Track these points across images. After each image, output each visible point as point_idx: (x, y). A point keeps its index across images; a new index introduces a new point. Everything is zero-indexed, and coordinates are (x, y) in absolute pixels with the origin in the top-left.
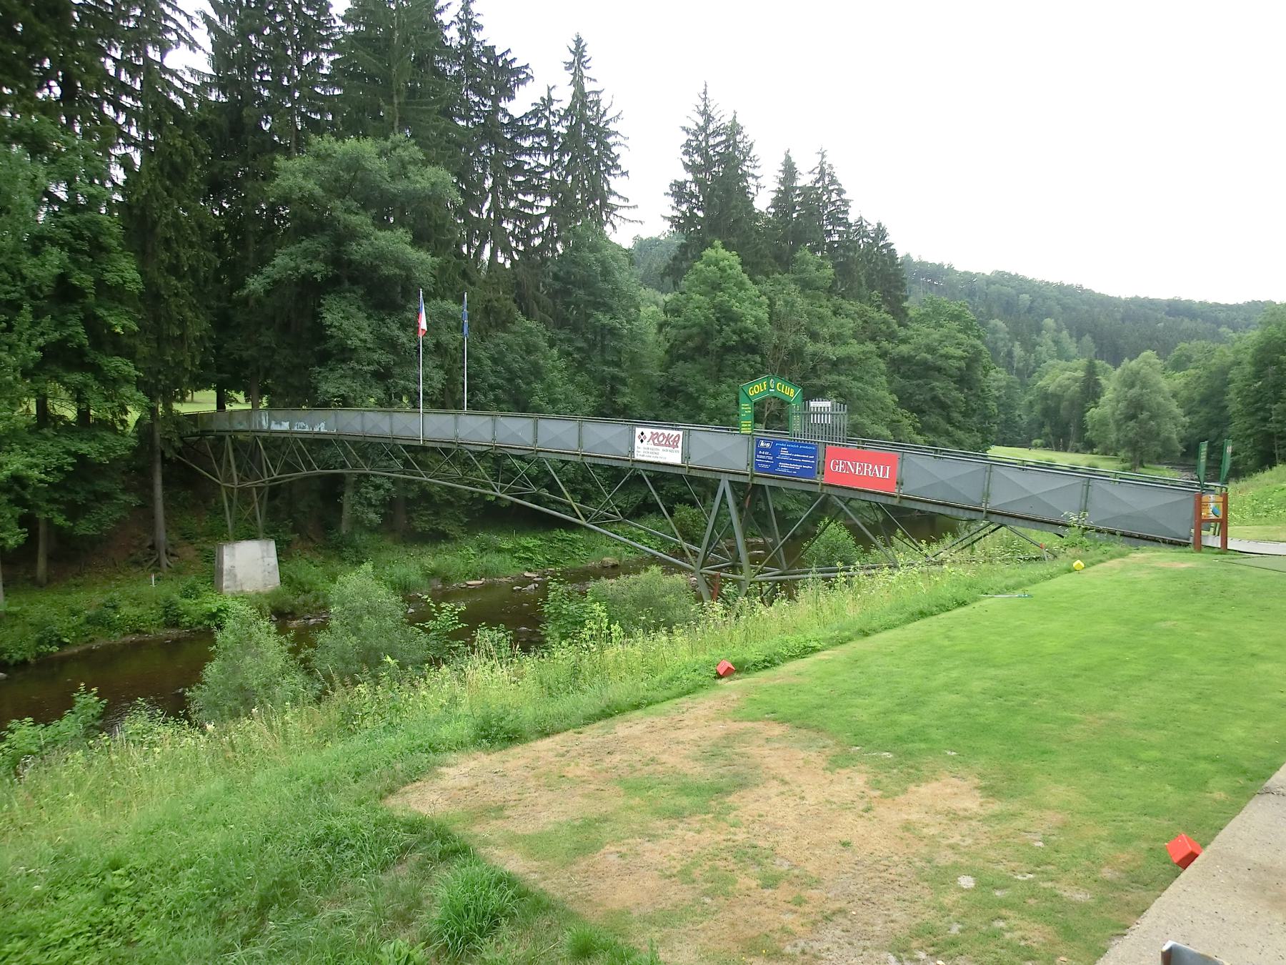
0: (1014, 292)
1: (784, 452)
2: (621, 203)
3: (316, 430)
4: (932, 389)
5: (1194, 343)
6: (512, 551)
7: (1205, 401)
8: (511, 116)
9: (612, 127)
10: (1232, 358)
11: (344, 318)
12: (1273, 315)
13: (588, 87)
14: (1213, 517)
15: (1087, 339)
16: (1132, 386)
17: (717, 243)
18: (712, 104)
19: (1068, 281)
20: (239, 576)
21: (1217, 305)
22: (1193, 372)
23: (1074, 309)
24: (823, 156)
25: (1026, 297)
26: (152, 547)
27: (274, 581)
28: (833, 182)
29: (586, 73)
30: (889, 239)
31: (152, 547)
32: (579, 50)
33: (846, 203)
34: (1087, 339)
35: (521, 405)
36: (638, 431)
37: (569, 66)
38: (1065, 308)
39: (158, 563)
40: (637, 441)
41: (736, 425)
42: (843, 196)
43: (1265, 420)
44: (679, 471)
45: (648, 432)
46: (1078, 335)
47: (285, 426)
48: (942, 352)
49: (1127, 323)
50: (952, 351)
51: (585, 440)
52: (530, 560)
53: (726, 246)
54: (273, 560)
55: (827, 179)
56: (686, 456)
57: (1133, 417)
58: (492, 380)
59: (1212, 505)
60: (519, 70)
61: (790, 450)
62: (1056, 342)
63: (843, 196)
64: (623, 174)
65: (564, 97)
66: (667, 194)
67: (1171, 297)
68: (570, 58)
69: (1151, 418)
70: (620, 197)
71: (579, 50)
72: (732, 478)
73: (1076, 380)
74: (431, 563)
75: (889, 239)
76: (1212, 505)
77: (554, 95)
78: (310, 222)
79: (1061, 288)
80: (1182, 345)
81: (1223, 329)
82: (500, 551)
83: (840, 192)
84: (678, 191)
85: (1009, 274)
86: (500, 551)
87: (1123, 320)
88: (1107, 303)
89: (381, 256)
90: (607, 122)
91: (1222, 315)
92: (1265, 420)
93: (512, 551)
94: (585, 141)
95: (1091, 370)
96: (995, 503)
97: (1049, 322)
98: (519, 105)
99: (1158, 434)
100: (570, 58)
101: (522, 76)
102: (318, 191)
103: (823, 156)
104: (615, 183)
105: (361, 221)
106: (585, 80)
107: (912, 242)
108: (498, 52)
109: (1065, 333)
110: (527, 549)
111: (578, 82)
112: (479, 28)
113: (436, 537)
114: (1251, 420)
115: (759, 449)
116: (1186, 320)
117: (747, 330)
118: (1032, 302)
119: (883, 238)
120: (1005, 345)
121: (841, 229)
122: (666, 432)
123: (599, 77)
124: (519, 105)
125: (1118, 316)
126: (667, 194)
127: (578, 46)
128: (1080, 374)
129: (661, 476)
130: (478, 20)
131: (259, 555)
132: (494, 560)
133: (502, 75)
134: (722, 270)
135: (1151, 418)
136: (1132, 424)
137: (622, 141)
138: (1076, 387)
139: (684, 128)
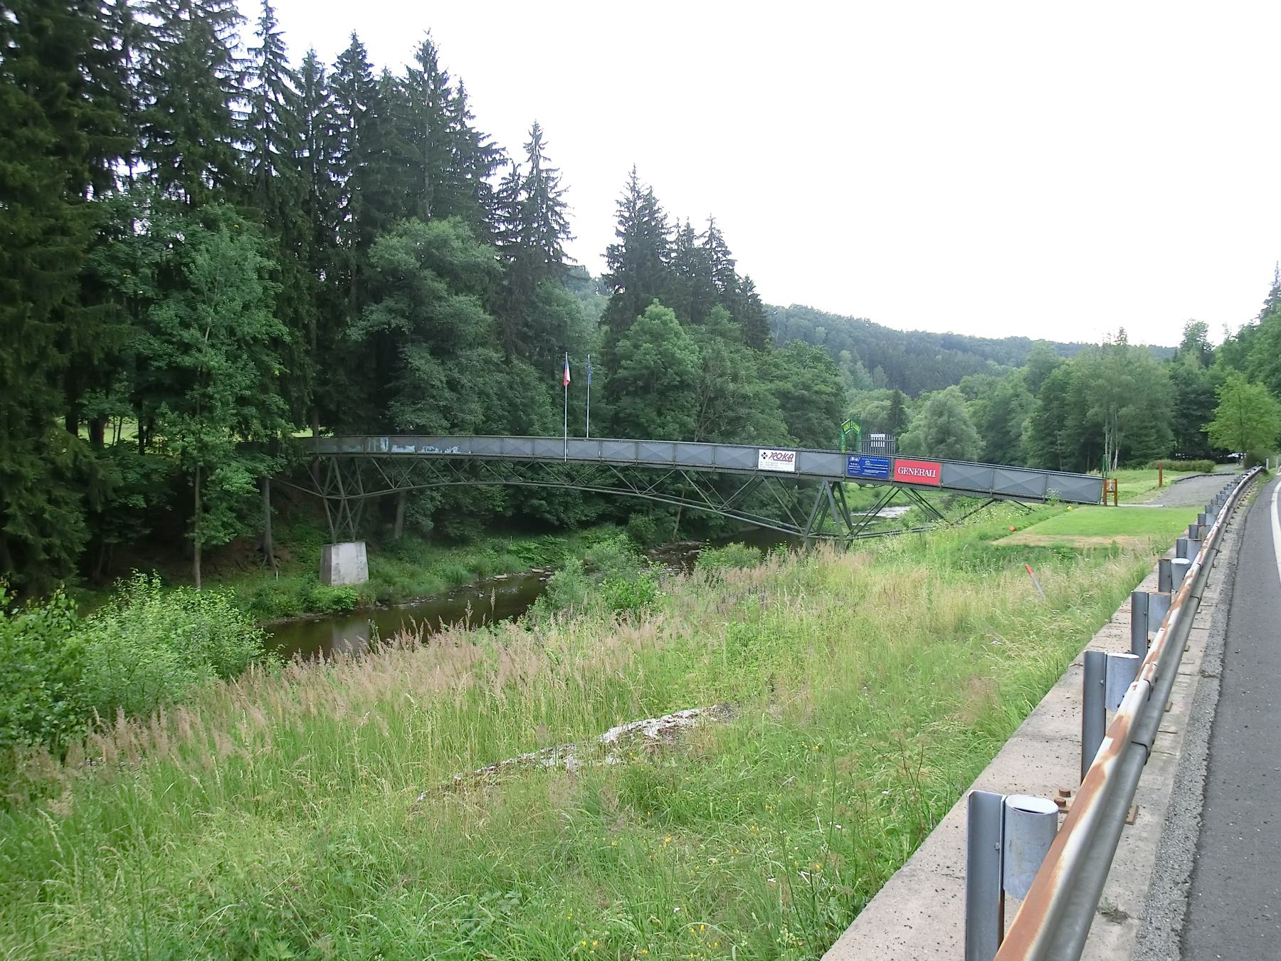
1: (868, 463)
3: (448, 452)
4: (808, 420)
5: (976, 376)
6: (517, 553)
7: (991, 427)
10: (1011, 391)
11: (420, 360)
12: (1039, 354)
13: (543, 165)
15: (879, 368)
16: (941, 415)
17: (656, 300)
19: (859, 313)
21: (984, 339)
22: (981, 402)
23: (864, 341)
25: (821, 329)
26: (261, 550)
28: (721, 244)
30: (756, 291)
31: (261, 550)
32: (536, 134)
33: (732, 263)
34: (879, 368)
35: (520, 430)
36: (761, 452)
38: (857, 341)
39: (269, 563)
40: (761, 459)
42: (729, 257)
43: (1053, 443)
45: (769, 452)
46: (871, 366)
47: (411, 449)
48: (816, 388)
49: (912, 355)
50: (823, 387)
52: (531, 559)
53: (664, 303)
54: (364, 559)
56: (796, 468)
57: (942, 441)
58: (500, 412)
60: (488, 151)
62: (853, 372)
63: (729, 257)
67: (945, 331)
68: (529, 140)
69: (956, 442)
71: (536, 134)
73: (883, 408)
74: (473, 560)
75: (756, 291)
78: (396, 282)
79: (850, 321)
80: (966, 378)
81: (990, 362)
82: (509, 552)
83: (726, 253)
85: (806, 308)
86: (509, 552)
87: (907, 352)
88: (891, 336)
89: (458, 315)
91: (988, 349)
92: (1053, 443)
93: (517, 553)
94: (537, 204)
95: (897, 401)
96: (997, 488)
97: (845, 353)
98: (496, 180)
99: (963, 455)
100: (529, 140)
101: (497, 157)
102: (413, 262)
105: (441, 286)
106: (541, 161)
107: (776, 290)
109: (859, 363)
110: (529, 550)
113: (461, 542)
114: (1042, 443)
116: (960, 353)
117: (687, 373)
124: (496, 180)
125: (903, 348)
127: (535, 131)
128: (888, 403)
132: (508, 559)
133: (485, 158)
134: (665, 323)
135: (956, 442)
136: (942, 447)
138: (884, 414)
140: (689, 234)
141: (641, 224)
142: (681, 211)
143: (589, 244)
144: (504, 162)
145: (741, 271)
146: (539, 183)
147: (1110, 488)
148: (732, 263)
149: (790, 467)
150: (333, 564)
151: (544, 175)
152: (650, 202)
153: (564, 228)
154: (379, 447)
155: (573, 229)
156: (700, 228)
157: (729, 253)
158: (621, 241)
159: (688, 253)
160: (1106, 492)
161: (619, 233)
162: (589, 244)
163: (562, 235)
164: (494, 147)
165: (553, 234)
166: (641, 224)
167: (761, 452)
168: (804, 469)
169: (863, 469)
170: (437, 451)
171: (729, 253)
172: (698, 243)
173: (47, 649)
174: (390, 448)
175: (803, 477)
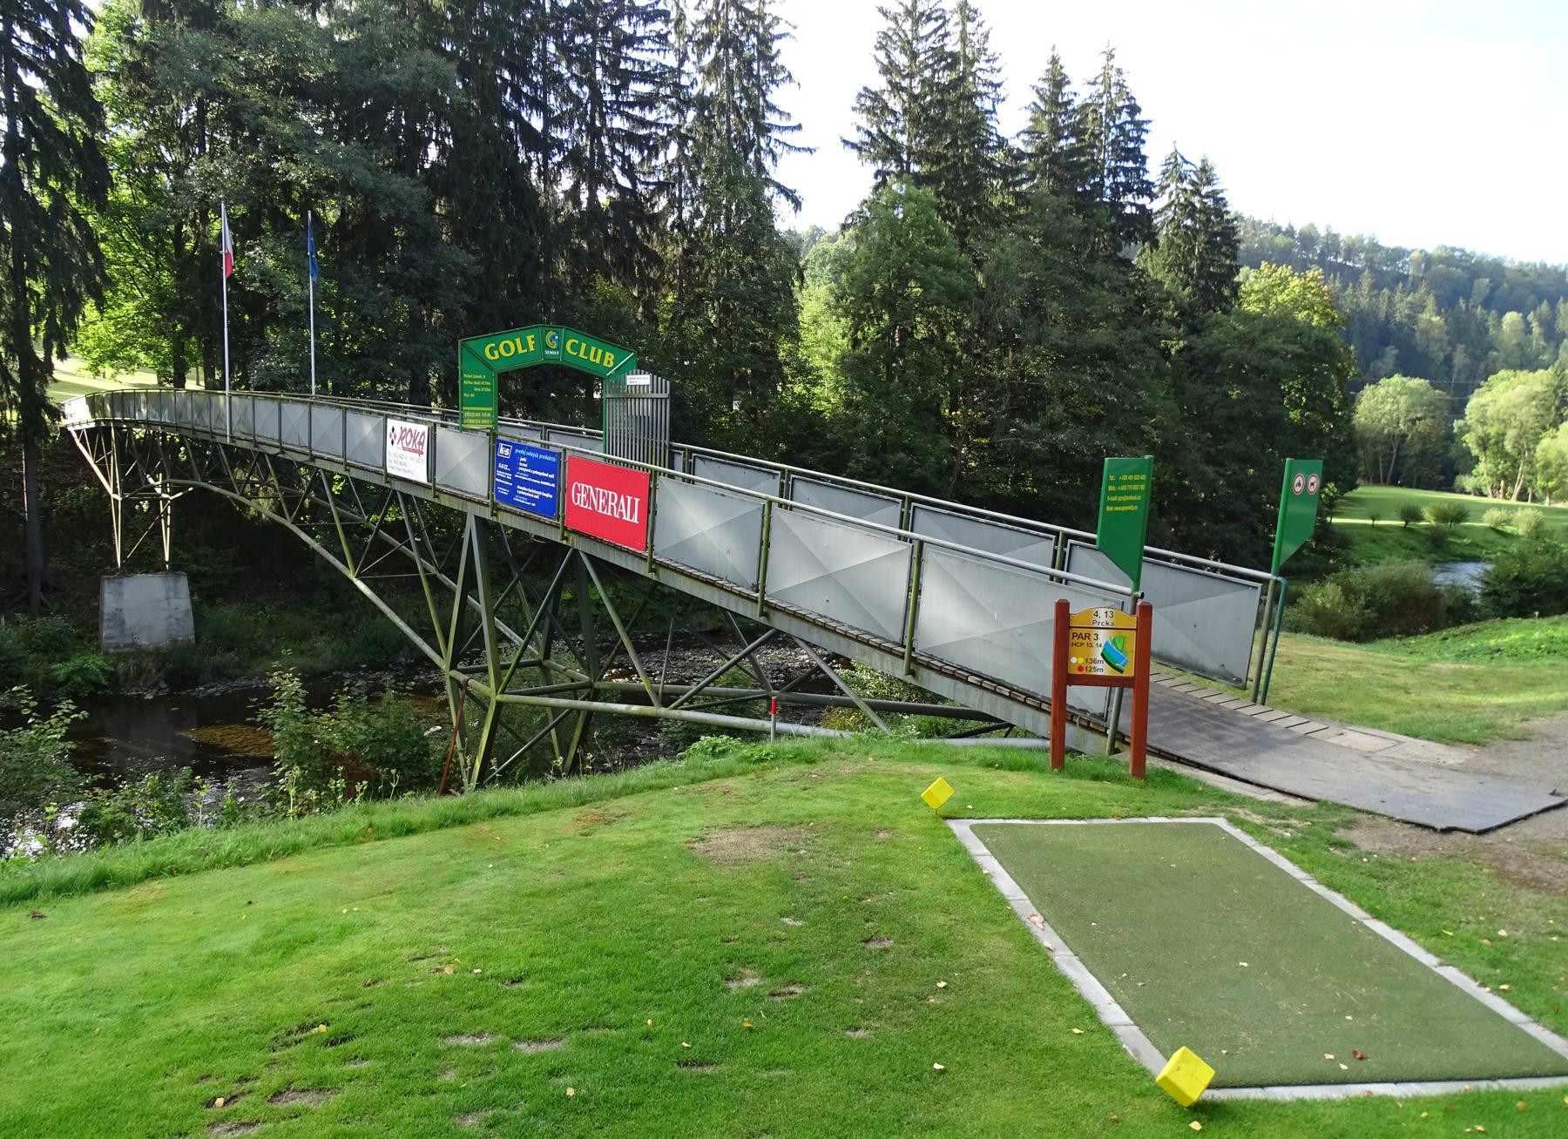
0: (1466, 275)
14: (1103, 670)
20: (129, 623)
26: (25, 577)
27: (186, 630)
33: (1139, 126)
42: (1138, 117)
54: (183, 602)
55: (1114, 90)
59: (1103, 637)
63: (1138, 117)
66: (854, 109)
70: (781, 113)
76: (1103, 637)
84: (874, 105)
103: (1111, 56)
104: (776, 95)
118: (1493, 289)
119: (1209, 182)
120: (1441, 349)
121: (1130, 164)
126: (854, 109)
131: (162, 594)
157: (1139, 110)
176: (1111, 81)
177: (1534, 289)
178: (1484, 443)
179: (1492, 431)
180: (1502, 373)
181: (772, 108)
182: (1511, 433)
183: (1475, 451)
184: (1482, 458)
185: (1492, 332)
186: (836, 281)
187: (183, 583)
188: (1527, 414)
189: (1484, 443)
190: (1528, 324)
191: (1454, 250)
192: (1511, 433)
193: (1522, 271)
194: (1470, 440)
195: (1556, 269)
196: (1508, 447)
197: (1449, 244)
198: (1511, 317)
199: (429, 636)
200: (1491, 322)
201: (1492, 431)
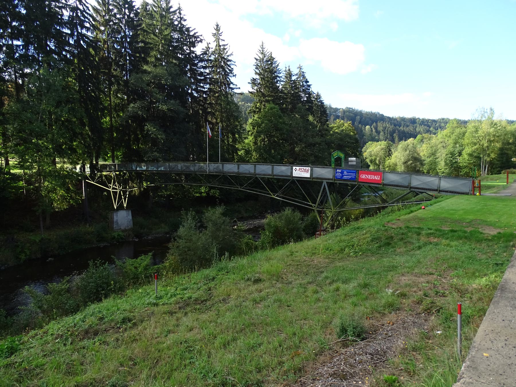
1: (345, 173)
2: (234, 87)
3: (159, 169)
8: (196, 54)
9: (229, 58)
18: (265, 50)
24: (301, 69)
29: (221, 37)
32: (218, 28)
33: (309, 86)
36: (294, 168)
37: (214, 35)
40: (294, 171)
41: (331, 165)
42: (308, 84)
44: (309, 180)
45: (298, 168)
51: (274, 171)
54: (130, 217)
56: (311, 174)
61: (347, 172)
63: (308, 84)
64: (234, 76)
65: (213, 46)
68: (215, 32)
71: (218, 28)
72: (327, 181)
77: (210, 46)
83: (307, 82)
90: (228, 56)
94: (221, 64)
98: (198, 50)
100: (215, 32)
106: (220, 41)
108: (190, 29)
111: (218, 40)
112: (185, 20)
115: (336, 172)
118: (361, 119)
119: (320, 98)
122: (304, 168)
123: (226, 38)
124: (198, 50)
129: (302, 181)
130: (185, 17)
133: (193, 40)
137: (233, 63)
139: (255, 58)
140: (289, 74)
141: (267, 69)
142: (286, 62)
143: (243, 80)
144: (201, 41)
145: (314, 89)
146: (220, 50)
147: (476, 185)
148: (309, 86)
149: (308, 175)
150: (115, 220)
151: (222, 47)
152: (271, 60)
153: (231, 71)
154: (132, 168)
155: (235, 72)
156: (295, 71)
157: (308, 82)
158: (258, 77)
159: (294, 85)
160: (474, 187)
161: (256, 73)
162: (243, 80)
163: (230, 75)
164: (197, 35)
165: (226, 75)
166: (267, 69)
167: (294, 168)
168: (314, 176)
169: (343, 176)
170: (155, 169)
171: (308, 82)
172: (294, 78)
173: (188, 251)
174: (136, 168)
175: (314, 180)
176: (302, 74)
177: (370, 119)
178: (371, 161)
179: (373, 158)
180: (369, 142)
181: (232, 83)
182: (378, 158)
183: (369, 164)
184: (371, 165)
185: (364, 131)
186: (490, 141)
187: (130, 212)
188: (381, 153)
189: (371, 161)
190: (371, 129)
191: (350, 108)
192: (378, 158)
193: (367, 114)
194: (368, 161)
195: (375, 113)
196: (377, 162)
197: (349, 107)
198: (368, 127)
199: (324, 188)
200: (363, 129)
201: (373, 158)
